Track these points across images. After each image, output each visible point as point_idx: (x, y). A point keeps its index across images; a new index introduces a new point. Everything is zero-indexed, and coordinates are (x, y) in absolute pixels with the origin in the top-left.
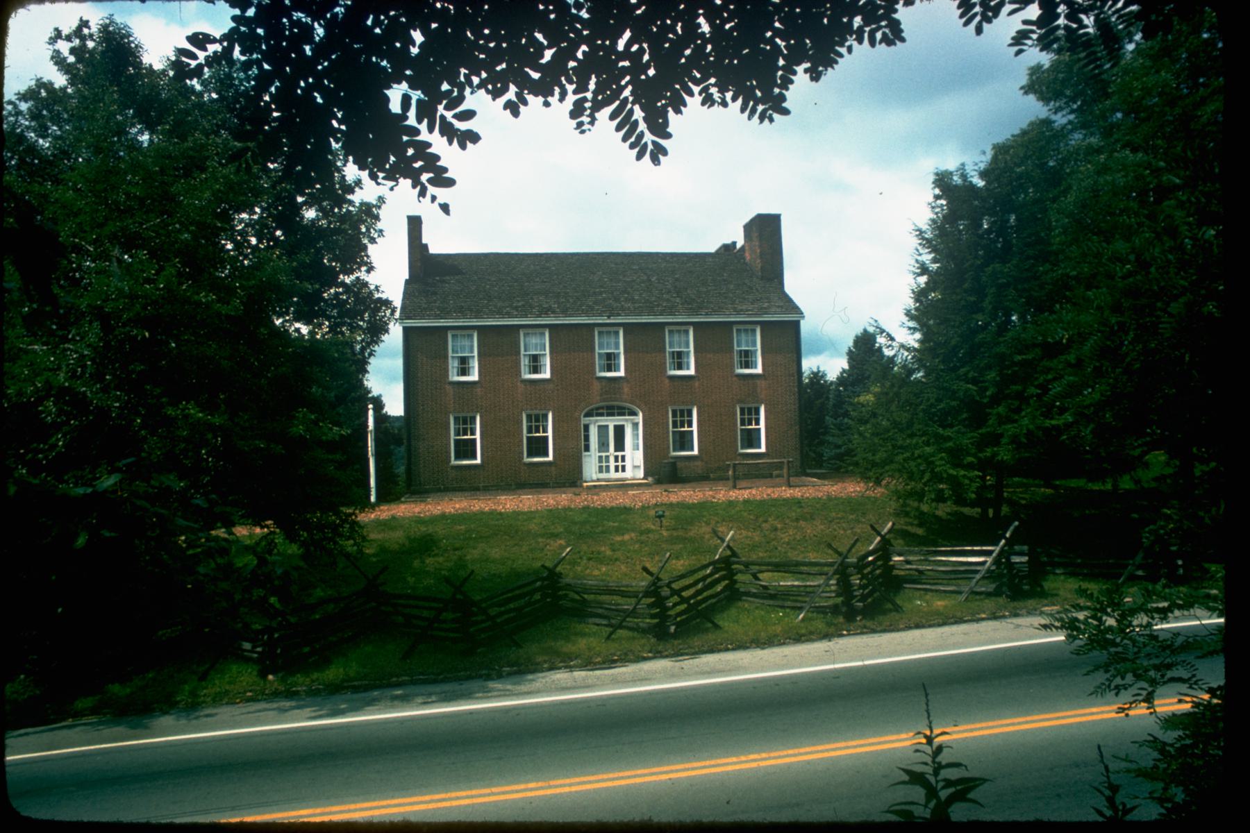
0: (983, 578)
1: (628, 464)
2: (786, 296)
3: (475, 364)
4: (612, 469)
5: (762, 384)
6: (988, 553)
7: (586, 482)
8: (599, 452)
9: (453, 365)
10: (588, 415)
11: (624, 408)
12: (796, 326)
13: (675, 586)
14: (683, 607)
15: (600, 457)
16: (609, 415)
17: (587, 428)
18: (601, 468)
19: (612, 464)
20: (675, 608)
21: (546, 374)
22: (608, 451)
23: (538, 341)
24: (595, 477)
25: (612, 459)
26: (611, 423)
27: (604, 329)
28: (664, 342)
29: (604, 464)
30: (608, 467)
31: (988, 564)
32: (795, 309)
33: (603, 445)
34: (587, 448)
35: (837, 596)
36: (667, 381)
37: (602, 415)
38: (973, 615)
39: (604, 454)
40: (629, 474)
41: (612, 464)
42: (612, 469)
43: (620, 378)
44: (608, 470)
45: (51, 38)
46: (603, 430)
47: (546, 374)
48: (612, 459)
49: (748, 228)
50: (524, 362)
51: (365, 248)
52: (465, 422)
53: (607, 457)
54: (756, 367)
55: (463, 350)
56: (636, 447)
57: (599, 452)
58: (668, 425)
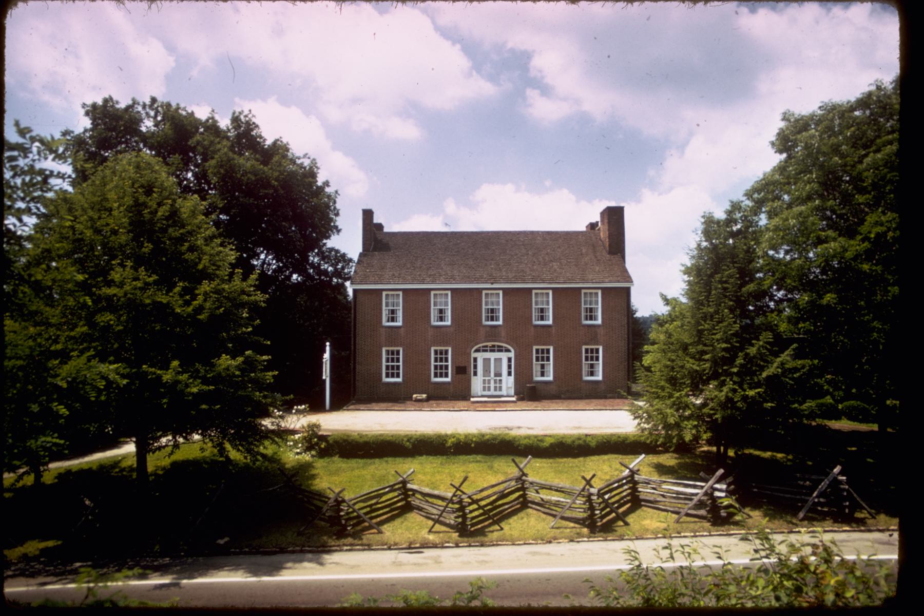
0: (695, 505)
1: (504, 388)
2: (626, 271)
3: (400, 314)
4: (492, 388)
5: (601, 332)
6: (702, 487)
7: (473, 397)
8: (484, 376)
9: (434, 314)
10: (477, 351)
11: (502, 347)
12: (627, 291)
13: (475, 497)
14: (481, 511)
15: (484, 381)
16: (491, 351)
17: (475, 360)
18: (484, 388)
19: (492, 385)
20: (473, 512)
21: (448, 323)
22: (490, 376)
23: (443, 300)
24: (480, 394)
25: (492, 382)
26: (493, 356)
27: (489, 292)
28: (531, 301)
29: (487, 385)
30: (489, 388)
31: (700, 495)
32: (628, 279)
33: (487, 371)
34: (475, 374)
35: (584, 512)
36: (532, 329)
37: (486, 351)
38: (679, 533)
39: (487, 378)
40: (504, 392)
41: (492, 385)
42: (492, 388)
43: (499, 326)
44: (489, 389)
45: (665, 296)
46: (487, 361)
47: (448, 323)
48: (492, 382)
49: (602, 214)
50: (534, 314)
51: (331, 220)
52: (441, 353)
53: (489, 381)
54: (549, 320)
55: (441, 304)
56: (509, 374)
57: (484, 376)
58: (532, 359)
